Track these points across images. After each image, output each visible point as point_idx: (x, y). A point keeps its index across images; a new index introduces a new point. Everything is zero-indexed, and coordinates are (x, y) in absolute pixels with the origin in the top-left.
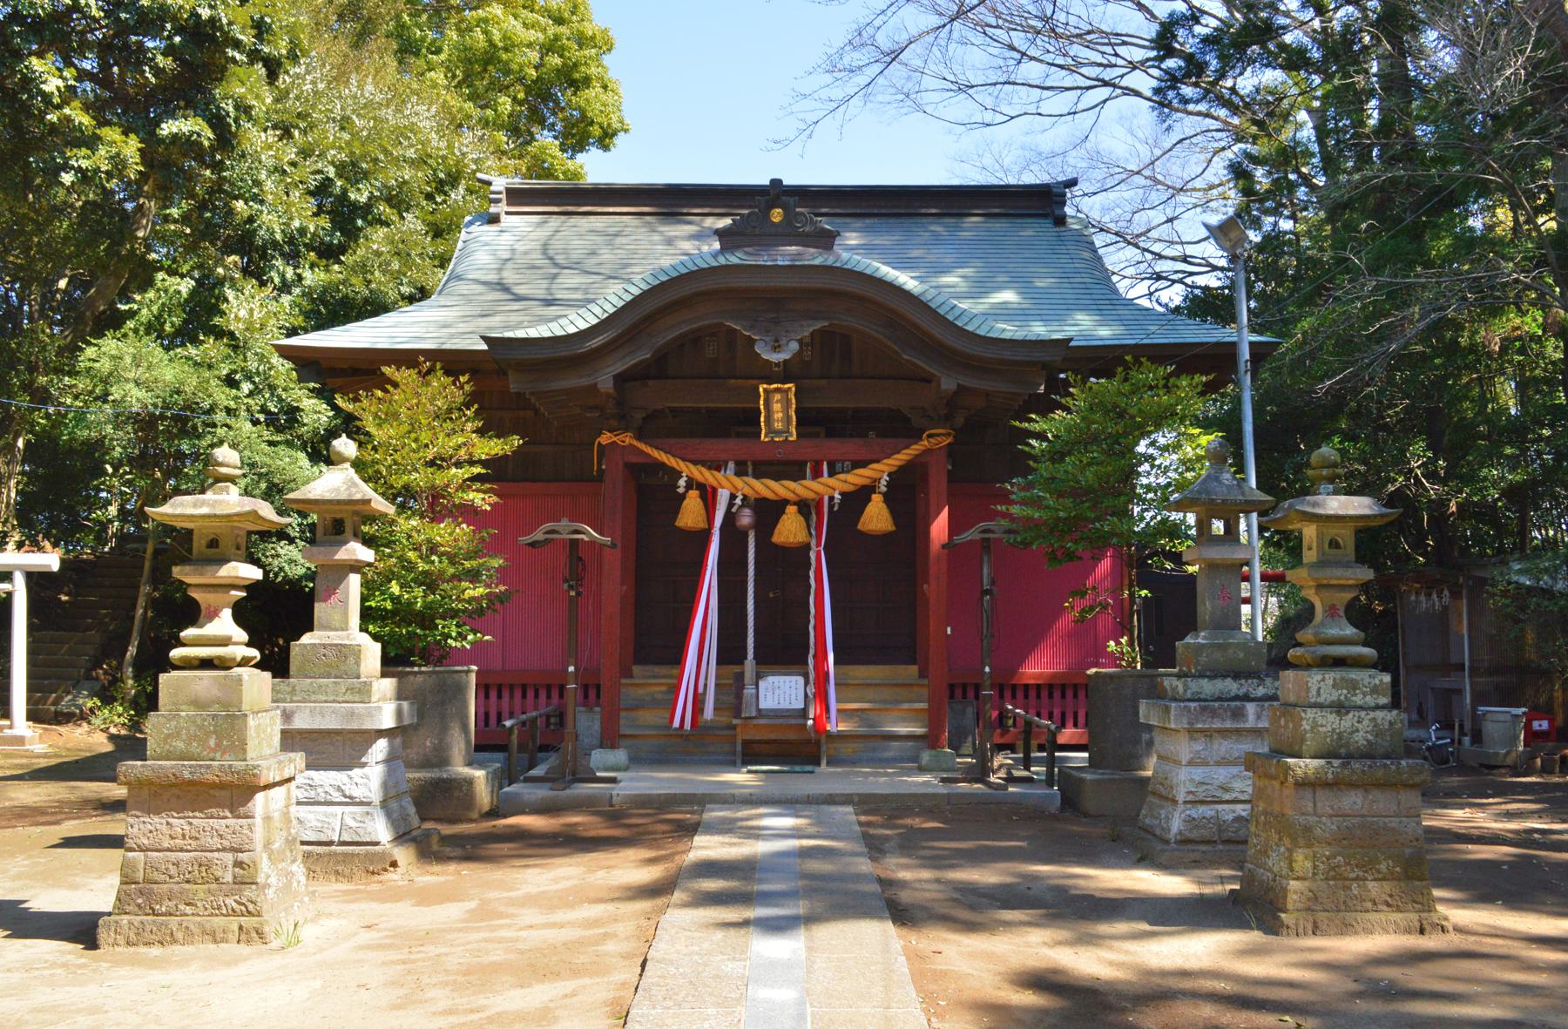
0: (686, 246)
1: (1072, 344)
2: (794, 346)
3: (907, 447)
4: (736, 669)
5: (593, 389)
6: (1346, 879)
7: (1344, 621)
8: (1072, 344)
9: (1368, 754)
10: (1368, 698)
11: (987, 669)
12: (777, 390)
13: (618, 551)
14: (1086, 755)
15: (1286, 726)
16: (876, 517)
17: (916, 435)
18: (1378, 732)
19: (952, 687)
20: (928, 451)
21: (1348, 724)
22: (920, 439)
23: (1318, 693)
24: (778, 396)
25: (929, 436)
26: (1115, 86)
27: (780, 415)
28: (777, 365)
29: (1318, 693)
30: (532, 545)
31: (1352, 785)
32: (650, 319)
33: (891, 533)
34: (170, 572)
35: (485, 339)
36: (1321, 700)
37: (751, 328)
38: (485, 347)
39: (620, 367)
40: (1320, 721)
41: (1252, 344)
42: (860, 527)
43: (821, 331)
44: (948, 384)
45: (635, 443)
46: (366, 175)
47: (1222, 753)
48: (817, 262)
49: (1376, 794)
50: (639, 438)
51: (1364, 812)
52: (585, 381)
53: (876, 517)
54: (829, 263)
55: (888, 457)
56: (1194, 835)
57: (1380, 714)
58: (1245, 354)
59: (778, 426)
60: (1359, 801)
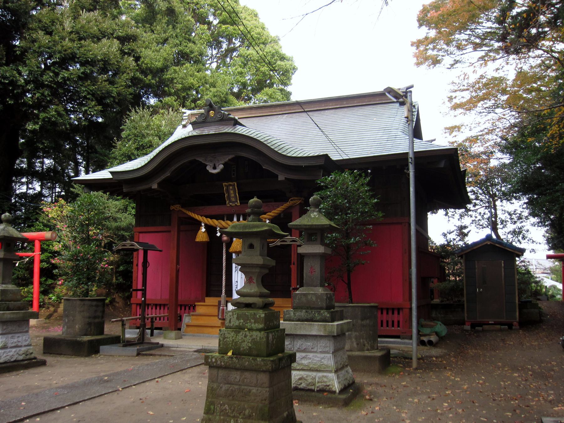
2: (221, 166)
3: (278, 207)
5: (150, 189)
6: (229, 416)
9: (249, 353)
10: (253, 325)
17: (286, 201)
18: (254, 342)
23: (230, 322)
24: (231, 187)
25: (292, 200)
27: (233, 195)
29: (230, 322)
32: (259, 153)
34: (276, 263)
37: (206, 160)
39: (159, 180)
40: (227, 335)
44: (281, 178)
45: (181, 209)
49: (247, 374)
51: (240, 383)
57: (255, 334)
60: (238, 377)
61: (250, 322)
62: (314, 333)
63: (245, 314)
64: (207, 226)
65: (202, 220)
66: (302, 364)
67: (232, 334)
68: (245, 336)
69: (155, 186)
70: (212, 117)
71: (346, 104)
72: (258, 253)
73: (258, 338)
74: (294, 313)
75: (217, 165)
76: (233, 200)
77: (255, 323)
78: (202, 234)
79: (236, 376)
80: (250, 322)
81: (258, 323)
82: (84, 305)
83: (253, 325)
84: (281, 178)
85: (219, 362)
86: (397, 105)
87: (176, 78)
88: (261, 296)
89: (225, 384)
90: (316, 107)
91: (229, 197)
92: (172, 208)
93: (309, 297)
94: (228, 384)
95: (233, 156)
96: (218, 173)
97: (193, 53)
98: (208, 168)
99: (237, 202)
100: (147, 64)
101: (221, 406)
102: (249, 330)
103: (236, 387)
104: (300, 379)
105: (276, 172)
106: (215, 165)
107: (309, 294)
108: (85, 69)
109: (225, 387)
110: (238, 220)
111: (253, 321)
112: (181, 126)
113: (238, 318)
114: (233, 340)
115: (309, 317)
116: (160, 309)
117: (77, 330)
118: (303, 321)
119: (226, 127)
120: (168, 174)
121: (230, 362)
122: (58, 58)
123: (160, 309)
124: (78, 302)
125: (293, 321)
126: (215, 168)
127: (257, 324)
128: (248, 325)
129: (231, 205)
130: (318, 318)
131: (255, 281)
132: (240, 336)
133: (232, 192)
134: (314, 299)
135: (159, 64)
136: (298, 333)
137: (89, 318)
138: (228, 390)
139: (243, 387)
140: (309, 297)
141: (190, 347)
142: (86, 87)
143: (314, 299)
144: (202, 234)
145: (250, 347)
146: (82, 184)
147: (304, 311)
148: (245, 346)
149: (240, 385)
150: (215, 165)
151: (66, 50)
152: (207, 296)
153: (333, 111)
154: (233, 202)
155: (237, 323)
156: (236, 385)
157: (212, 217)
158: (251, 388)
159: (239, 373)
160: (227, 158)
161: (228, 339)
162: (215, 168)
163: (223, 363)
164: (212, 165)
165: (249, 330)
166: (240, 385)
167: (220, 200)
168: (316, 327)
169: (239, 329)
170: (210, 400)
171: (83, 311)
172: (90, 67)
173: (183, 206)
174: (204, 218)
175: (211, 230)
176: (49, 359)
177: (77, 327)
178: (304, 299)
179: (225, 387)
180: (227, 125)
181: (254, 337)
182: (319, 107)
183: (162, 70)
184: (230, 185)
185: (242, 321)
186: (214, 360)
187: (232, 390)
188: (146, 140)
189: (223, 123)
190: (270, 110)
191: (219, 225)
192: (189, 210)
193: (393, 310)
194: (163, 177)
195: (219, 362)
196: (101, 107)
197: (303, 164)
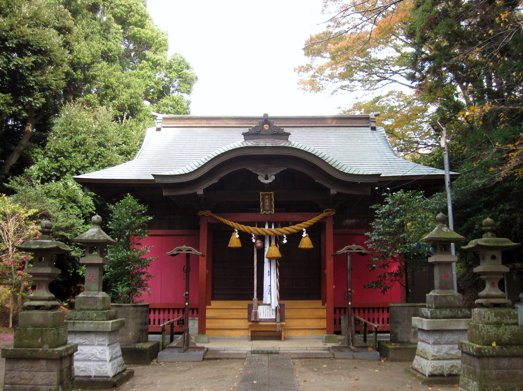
0: (234, 141)
1: (381, 175)
2: (273, 177)
4: (249, 302)
7: (498, 289)
8: (381, 175)
10: (509, 321)
11: (350, 303)
12: (267, 194)
13: (205, 258)
14: (389, 335)
15: (476, 332)
16: (306, 242)
19: (335, 309)
20: (325, 217)
21: (501, 331)
22: (322, 212)
23: (489, 319)
24: (267, 197)
25: (326, 212)
26: (390, 79)
27: (268, 204)
28: (267, 184)
29: (489, 319)
30: (173, 255)
31: (504, 356)
33: (311, 249)
35: (154, 175)
36: (490, 321)
38: (153, 178)
39: (206, 186)
40: (490, 330)
41: (451, 175)
42: (299, 247)
43: (284, 171)
44: (333, 191)
45: (212, 215)
46: (414, 31)
47: (446, 340)
48: (282, 145)
49: (514, 360)
50: (212, 212)
52: (192, 192)
53: (306, 242)
54: (287, 145)
55: (310, 219)
56: (436, 372)
58: (447, 179)
59: (267, 208)
60: (506, 363)
61: (506, 318)
62: (462, 327)
63: (502, 312)
64: (240, 232)
65: (300, 228)
66: (451, 354)
67: (495, 329)
68: (506, 330)
69: (200, 192)
70: (265, 131)
71: (320, 124)
72: (501, 262)
73: (516, 331)
74: (440, 312)
75: (269, 176)
76: (267, 208)
77: (510, 319)
78: (235, 241)
79: (504, 362)
80: (506, 318)
81: (512, 319)
82: (137, 311)
83: (509, 321)
84: (333, 191)
85: (491, 352)
86: (369, 129)
87: (99, 76)
88: (50, 299)
89: (495, 369)
90: (292, 124)
91: (263, 205)
92: (200, 213)
93: (448, 298)
94: (498, 369)
95: (286, 168)
96: (270, 183)
97: (112, 51)
98: (259, 178)
99: (271, 210)
100: (79, 59)
101: (494, 387)
102: (506, 324)
103: (505, 371)
104: (452, 367)
105: (328, 186)
106: (266, 175)
107: (448, 296)
108: (37, 58)
109: (494, 372)
110: (270, 227)
111: (508, 317)
112: (155, 128)
113: (496, 316)
114: (495, 334)
115: (453, 314)
116: (174, 313)
117: (131, 338)
118: (447, 318)
119: (281, 141)
120: (215, 181)
121: (501, 351)
122: (15, 44)
123: (174, 313)
124: (131, 309)
125: (439, 318)
126: (267, 178)
127: (512, 320)
128: (505, 321)
129: (265, 213)
130: (461, 315)
131: (497, 285)
132: (501, 330)
133: (267, 201)
134: (453, 299)
135: (88, 60)
136: (449, 328)
137: (142, 324)
138: (498, 374)
139: (511, 370)
140: (448, 298)
141: (237, 349)
142: (34, 77)
143: (453, 299)
144: (235, 241)
145: (509, 338)
146: (79, 183)
147: (448, 310)
148: (506, 338)
149: (508, 369)
150: (266, 175)
151: (23, 37)
152: (213, 299)
153: (310, 129)
154: (267, 211)
155: (495, 320)
156: (504, 369)
157: (246, 224)
158: (517, 370)
159: (506, 359)
160: (279, 170)
161: (491, 333)
162: (267, 178)
163: (495, 353)
164: (264, 175)
165: (506, 324)
166: (508, 369)
167: (255, 207)
168: (463, 323)
169: (498, 324)
170: (483, 384)
171: (136, 318)
172: (41, 57)
173: (213, 212)
174: (238, 225)
175: (245, 237)
176: (138, 369)
177: (130, 334)
178: (444, 300)
179: (494, 372)
180: (281, 139)
181: (513, 330)
182: (295, 124)
183: (89, 66)
184: (267, 194)
185: (499, 318)
186: (486, 351)
187: (502, 374)
188: (80, 137)
189: (278, 136)
190: (247, 122)
191: (255, 232)
192: (218, 215)
193: (373, 309)
194: (209, 184)
195: (491, 352)
196: (44, 99)
197: (206, 170)
